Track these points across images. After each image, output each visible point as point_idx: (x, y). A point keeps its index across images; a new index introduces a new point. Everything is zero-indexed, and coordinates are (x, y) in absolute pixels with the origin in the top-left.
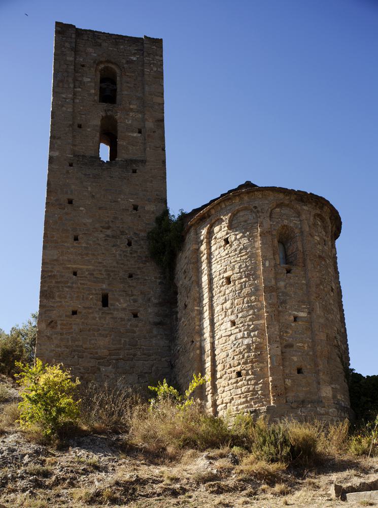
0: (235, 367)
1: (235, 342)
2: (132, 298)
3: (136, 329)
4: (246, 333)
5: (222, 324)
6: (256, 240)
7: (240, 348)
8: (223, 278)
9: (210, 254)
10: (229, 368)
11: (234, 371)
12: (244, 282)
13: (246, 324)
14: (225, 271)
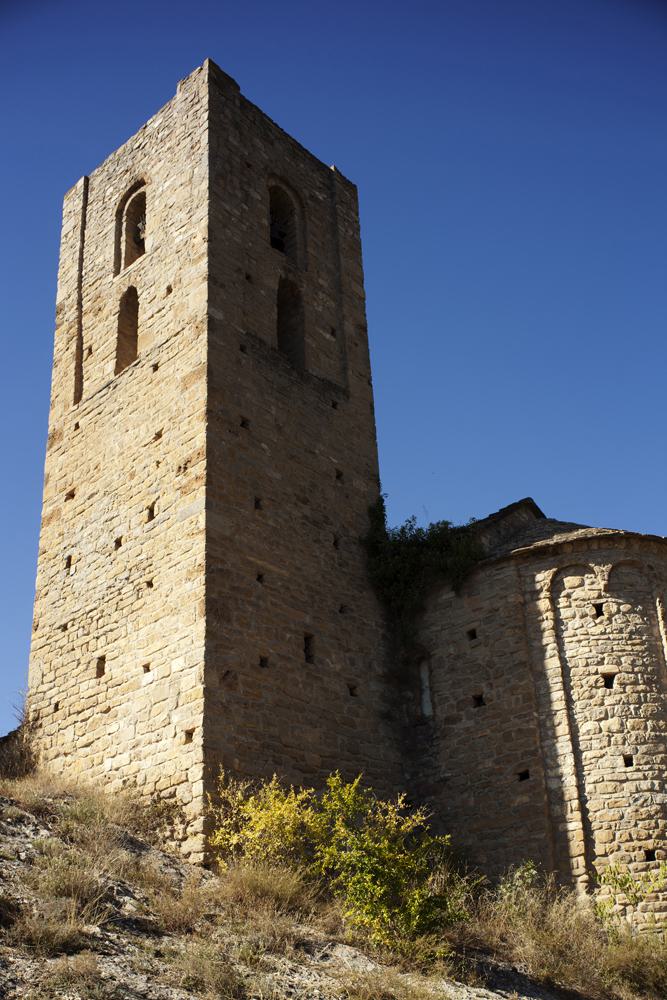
0: (640, 840)
1: (637, 796)
2: (347, 655)
3: (357, 720)
4: (656, 782)
5: (601, 757)
6: (653, 622)
7: (649, 808)
8: (596, 673)
9: (558, 623)
10: (627, 841)
11: (640, 848)
12: (643, 691)
13: (656, 767)
14: (601, 663)
